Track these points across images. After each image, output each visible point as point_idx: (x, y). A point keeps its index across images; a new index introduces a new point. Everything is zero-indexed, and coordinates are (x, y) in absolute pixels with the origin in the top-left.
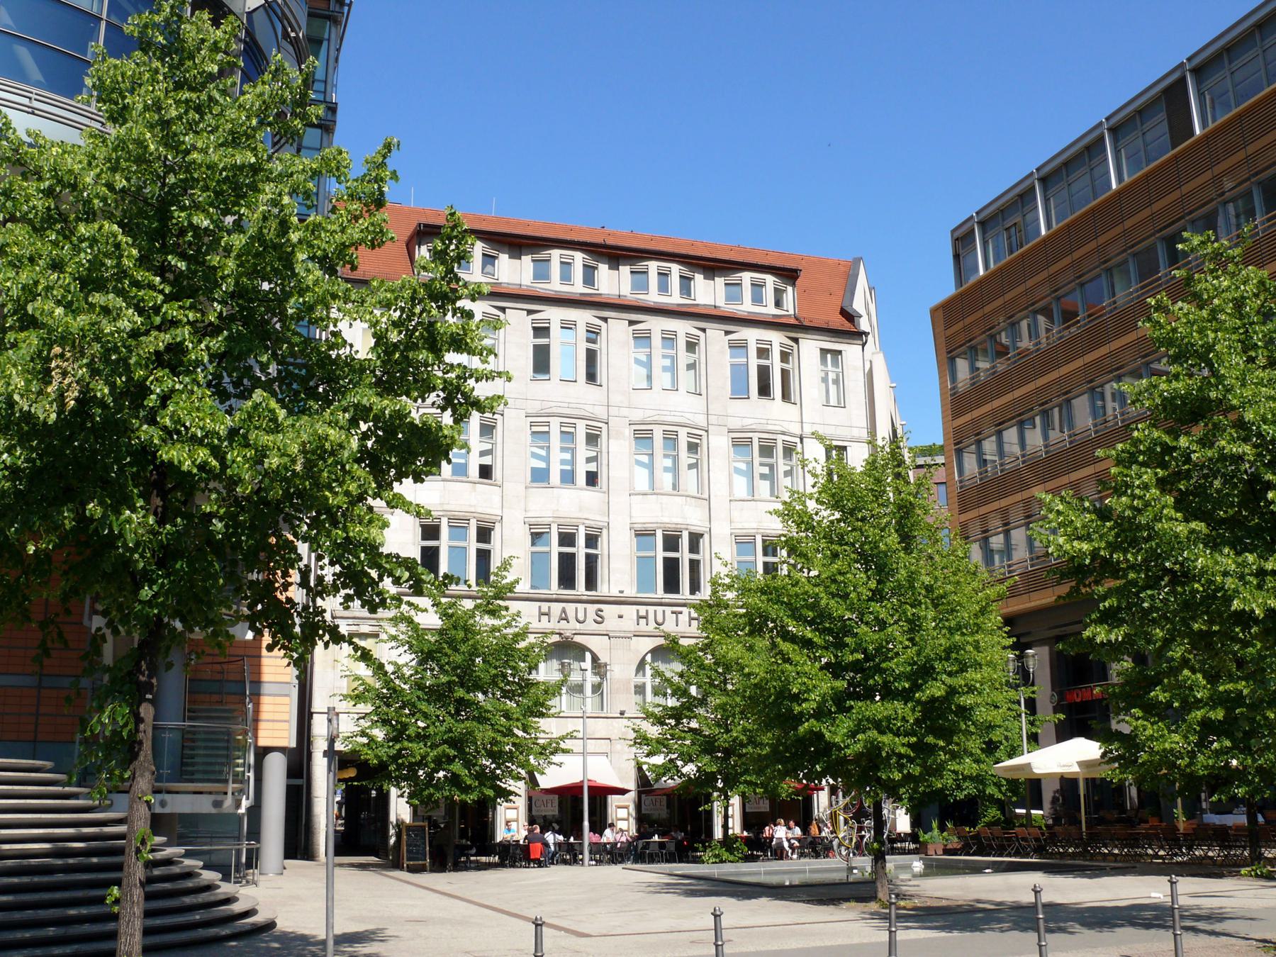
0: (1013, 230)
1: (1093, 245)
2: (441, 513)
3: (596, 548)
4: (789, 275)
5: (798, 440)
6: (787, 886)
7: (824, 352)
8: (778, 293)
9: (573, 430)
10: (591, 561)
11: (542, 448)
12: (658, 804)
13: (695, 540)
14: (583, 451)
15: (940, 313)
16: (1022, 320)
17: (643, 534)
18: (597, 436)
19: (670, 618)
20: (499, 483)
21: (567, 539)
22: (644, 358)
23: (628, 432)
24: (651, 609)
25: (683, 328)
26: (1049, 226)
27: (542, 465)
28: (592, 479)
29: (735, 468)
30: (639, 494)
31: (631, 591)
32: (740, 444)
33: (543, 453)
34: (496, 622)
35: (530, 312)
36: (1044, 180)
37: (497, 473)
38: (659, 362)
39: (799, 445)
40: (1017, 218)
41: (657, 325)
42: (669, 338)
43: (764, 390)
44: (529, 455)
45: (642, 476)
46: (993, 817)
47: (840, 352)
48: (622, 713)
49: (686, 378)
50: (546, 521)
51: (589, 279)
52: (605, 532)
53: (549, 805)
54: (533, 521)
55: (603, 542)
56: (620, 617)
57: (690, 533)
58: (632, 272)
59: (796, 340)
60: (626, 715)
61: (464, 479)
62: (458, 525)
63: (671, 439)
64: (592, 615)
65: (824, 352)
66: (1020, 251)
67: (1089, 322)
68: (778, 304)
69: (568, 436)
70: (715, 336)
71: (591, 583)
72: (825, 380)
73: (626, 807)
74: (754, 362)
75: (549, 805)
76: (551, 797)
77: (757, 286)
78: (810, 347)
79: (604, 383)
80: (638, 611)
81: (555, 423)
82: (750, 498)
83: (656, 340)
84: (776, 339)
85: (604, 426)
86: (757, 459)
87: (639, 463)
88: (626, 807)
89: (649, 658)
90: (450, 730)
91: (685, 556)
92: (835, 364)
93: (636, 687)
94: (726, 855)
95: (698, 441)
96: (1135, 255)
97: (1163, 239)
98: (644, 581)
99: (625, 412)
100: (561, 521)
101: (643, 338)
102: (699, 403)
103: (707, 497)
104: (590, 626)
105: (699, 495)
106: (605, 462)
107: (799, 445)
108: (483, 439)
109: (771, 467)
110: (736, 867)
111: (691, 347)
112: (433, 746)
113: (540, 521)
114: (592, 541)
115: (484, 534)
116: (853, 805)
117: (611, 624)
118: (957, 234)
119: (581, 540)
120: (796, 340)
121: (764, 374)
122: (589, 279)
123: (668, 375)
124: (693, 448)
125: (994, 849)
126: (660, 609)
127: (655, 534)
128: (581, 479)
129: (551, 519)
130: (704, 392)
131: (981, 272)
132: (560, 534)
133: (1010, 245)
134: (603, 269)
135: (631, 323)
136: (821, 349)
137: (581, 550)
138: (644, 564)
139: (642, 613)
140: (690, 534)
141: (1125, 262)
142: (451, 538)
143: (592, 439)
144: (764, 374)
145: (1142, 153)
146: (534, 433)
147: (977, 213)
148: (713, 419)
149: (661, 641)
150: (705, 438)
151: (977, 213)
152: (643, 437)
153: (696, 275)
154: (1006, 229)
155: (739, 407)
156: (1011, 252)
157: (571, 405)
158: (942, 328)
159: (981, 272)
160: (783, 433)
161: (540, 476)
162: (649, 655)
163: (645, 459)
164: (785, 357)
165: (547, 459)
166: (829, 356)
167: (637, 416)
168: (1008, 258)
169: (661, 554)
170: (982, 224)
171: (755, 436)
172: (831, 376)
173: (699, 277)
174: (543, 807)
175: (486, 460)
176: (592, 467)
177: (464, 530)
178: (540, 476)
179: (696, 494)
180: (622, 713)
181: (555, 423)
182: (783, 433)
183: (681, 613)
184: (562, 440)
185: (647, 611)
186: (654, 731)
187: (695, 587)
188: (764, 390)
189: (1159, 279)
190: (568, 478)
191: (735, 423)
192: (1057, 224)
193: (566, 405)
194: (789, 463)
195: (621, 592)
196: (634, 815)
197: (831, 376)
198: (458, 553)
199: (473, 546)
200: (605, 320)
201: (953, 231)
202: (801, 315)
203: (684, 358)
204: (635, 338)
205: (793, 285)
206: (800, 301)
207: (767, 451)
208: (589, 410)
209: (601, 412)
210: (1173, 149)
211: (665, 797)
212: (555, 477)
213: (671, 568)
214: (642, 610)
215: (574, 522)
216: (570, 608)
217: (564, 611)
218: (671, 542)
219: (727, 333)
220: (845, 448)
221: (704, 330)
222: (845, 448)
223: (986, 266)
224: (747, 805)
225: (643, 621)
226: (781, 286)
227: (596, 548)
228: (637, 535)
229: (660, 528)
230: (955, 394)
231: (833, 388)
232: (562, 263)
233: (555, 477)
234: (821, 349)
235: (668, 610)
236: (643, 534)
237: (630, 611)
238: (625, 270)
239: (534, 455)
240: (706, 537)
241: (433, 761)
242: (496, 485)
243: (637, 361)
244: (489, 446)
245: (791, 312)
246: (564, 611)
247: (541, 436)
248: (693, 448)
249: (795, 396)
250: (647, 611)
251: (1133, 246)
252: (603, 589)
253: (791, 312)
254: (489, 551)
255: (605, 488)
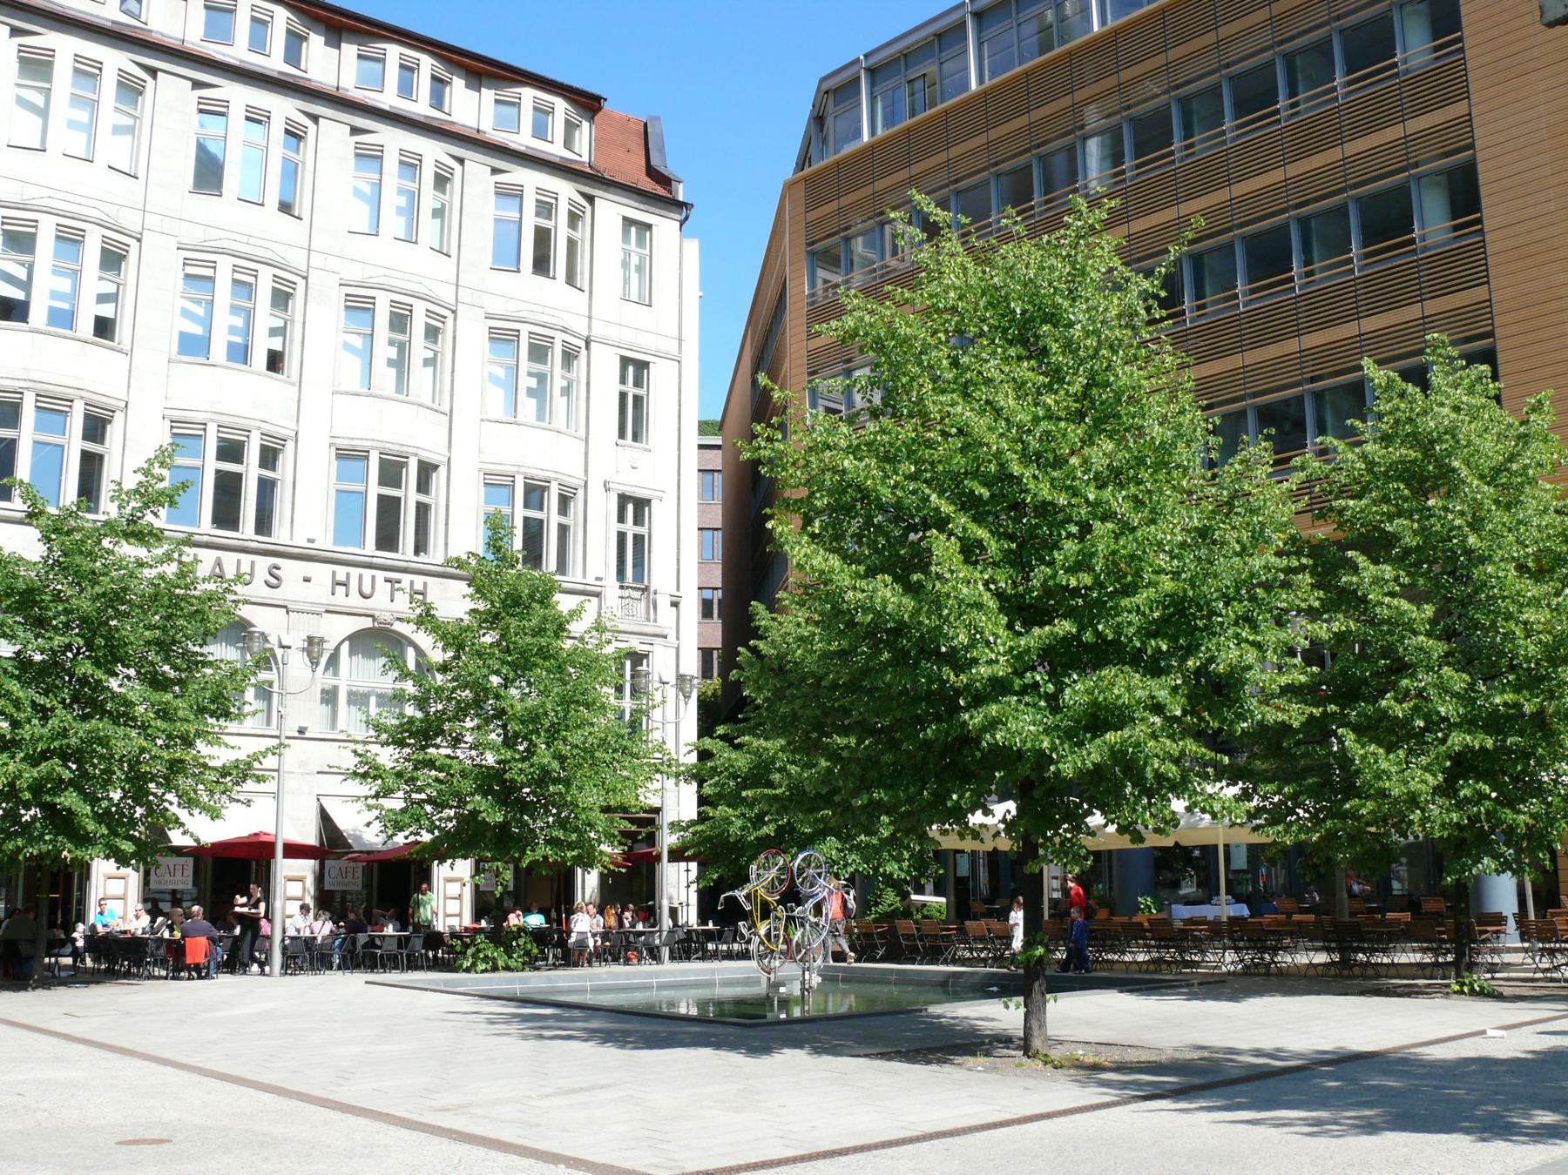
0: (919, 85)
1: (1209, 38)
2: (24, 384)
3: (274, 469)
4: (588, 103)
5: (582, 344)
6: (687, 1019)
7: (628, 222)
8: (570, 127)
9: (252, 280)
10: (266, 489)
11: (198, 302)
12: (350, 875)
13: (426, 471)
14: (265, 317)
15: (800, 190)
16: (858, 235)
17: (349, 456)
18: (288, 296)
19: (383, 589)
20: (127, 347)
21: (231, 451)
22: (367, 189)
23: (337, 297)
24: (355, 572)
25: (433, 151)
26: (981, 80)
27: (197, 330)
28: (275, 361)
29: (490, 373)
30: (347, 393)
31: (325, 542)
32: (502, 337)
33: (200, 311)
34: (141, 552)
35: (197, 85)
36: (872, 72)
37: (123, 331)
38: (392, 199)
39: (584, 352)
40: (930, 68)
41: (394, 140)
42: (410, 165)
43: (542, 264)
44: (178, 311)
45: (352, 367)
46: (890, 906)
47: (649, 227)
48: (301, 731)
49: (429, 228)
50: (200, 417)
51: (293, 54)
52: (290, 445)
53: (178, 873)
54: (177, 415)
55: (285, 461)
56: (307, 580)
57: (420, 461)
58: (360, 56)
59: (590, 199)
60: (307, 735)
61: (68, 332)
62: (53, 407)
63: (399, 322)
64: (262, 574)
65: (628, 222)
66: (1063, 48)
67: (1046, 210)
68: (568, 144)
69: (244, 288)
70: (477, 172)
71: (264, 523)
72: (625, 264)
73: (301, 880)
74: (530, 222)
75: (178, 873)
76: (181, 860)
77: (542, 112)
78: (610, 211)
79: (306, 215)
80: (334, 573)
81: (225, 265)
82: (511, 419)
83: (391, 163)
84: (566, 191)
85: (301, 283)
86: (525, 365)
87: (348, 347)
88: (301, 880)
89: (345, 647)
90: (64, 733)
91: (409, 496)
92: (641, 242)
93: (323, 691)
94: (498, 954)
95: (440, 325)
96: (958, 192)
97: (1180, 100)
98: (346, 526)
99: (334, 263)
100: (225, 420)
101: (370, 157)
102: (446, 267)
103: (447, 410)
104: (258, 590)
105: (435, 406)
106: (297, 337)
107: (584, 352)
108: (108, 275)
109: (541, 378)
110: (522, 981)
111: (441, 181)
112: (34, 760)
113: (190, 416)
114: (269, 457)
115: (95, 427)
116: (781, 882)
117: (287, 592)
118: (825, 87)
119: (253, 454)
120: (590, 199)
121: (543, 238)
122: (293, 54)
123: (402, 221)
124: (432, 333)
125: (918, 953)
126: (368, 573)
127: (367, 458)
128: (260, 359)
129: (208, 416)
130: (454, 252)
131: (866, 137)
132: (220, 440)
133: (912, 105)
134: (316, 41)
135: (355, 131)
136: (625, 219)
137: (251, 470)
138: (347, 502)
139: (341, 577)
140: (421, 463)
141: (987, 183)
142: (39, 427)
143: (281, 299)
144: (543, 238)
145: (1015, 48)
146: (188, 276)
147: (866, 56)
148: (464, 295)
149: (367, 623)
150: (450, 321)
151: (866, 56)
152: (358, 306)
153: (455, 78)
154: (909, 82)
155: (504, 282)
156: (913, 114)
157: (252, 241)
158: (803, 209)
159: (866, 137)
160: (564, 330)
161: (194, 347)
162: (347, 644)
163: (357, 342)
164: (574, 219)
165: (208, 323)
166: (633, 230)
167: (354, 273)
168: (909, 122)
169: (374, 490)
170: (872, 72)
171: (525, 330)
172: (635, 260)
173: (458, 83)
174: (167, 877)
175: (107, 311)
176: (276, 344)
177: (60, 418)
178: (194, 347)
179: (429, 403)
180: (301, 731)
181: (225, 265)
182: (564, 330)
183: (399, 582)
184: (234, 294)
185: (348, 575)
186: (387, 757)
187: (420, 547)
188: (542, 264)
189: (1032, 208)
190: (240, 354)
191: (498, 307)
192: (990, 79)
193: (244, 239)
194: (568, 375)
195: (311, 541)
196: (312, 892)
197: (635, 260)
198: (50, 454)
199: (76, 445)
200: (315, 118)
201: (824, 79)
202: (601, 165)
203: (429, 198)
204: (357, 155)
205: (591, 119)
206: (598, 144)
207: (539, 352)
208: (279, 252)
209: (297, 259)
210: (1041, 55)
211: (190, 861)
212: (219, 351)
213: (389, 510)
214: (341, 572)
215: (245, 423)
216: (229, 559)
217: (219, 563)
218: (391, 472)
219: (495, 171)
220: (646, 365)
221: (461, 161)
222: (646, 365)
223: (873, 132)
224: (153, 877)
225: (341, 590)
226: (575, 117)
227: (274, 469)
228: (339, 457)
229: (377, 448)
230: (813, 303)
231: (634, 277)
232: (254, 19)
233: (219, 351)
234: (625, 219)
235: (381, 575)
236: (349, 456)
237: (322, 572)
238: (350, 50)
239: (186, 313)
240: (443, 470)
241: (29, 788)
242: (120, 351)
243: (358, 193)
244: (111, 288)
245: (585, 159)
246: (219, 563)
247: (200, 282)
248: (432, 333)
249: (582, 279)
250: (348, 575)
251: (957, 181)
252: (281, 535)
253: (585, 159)
254: (101, 457)
255: (295, 378)
